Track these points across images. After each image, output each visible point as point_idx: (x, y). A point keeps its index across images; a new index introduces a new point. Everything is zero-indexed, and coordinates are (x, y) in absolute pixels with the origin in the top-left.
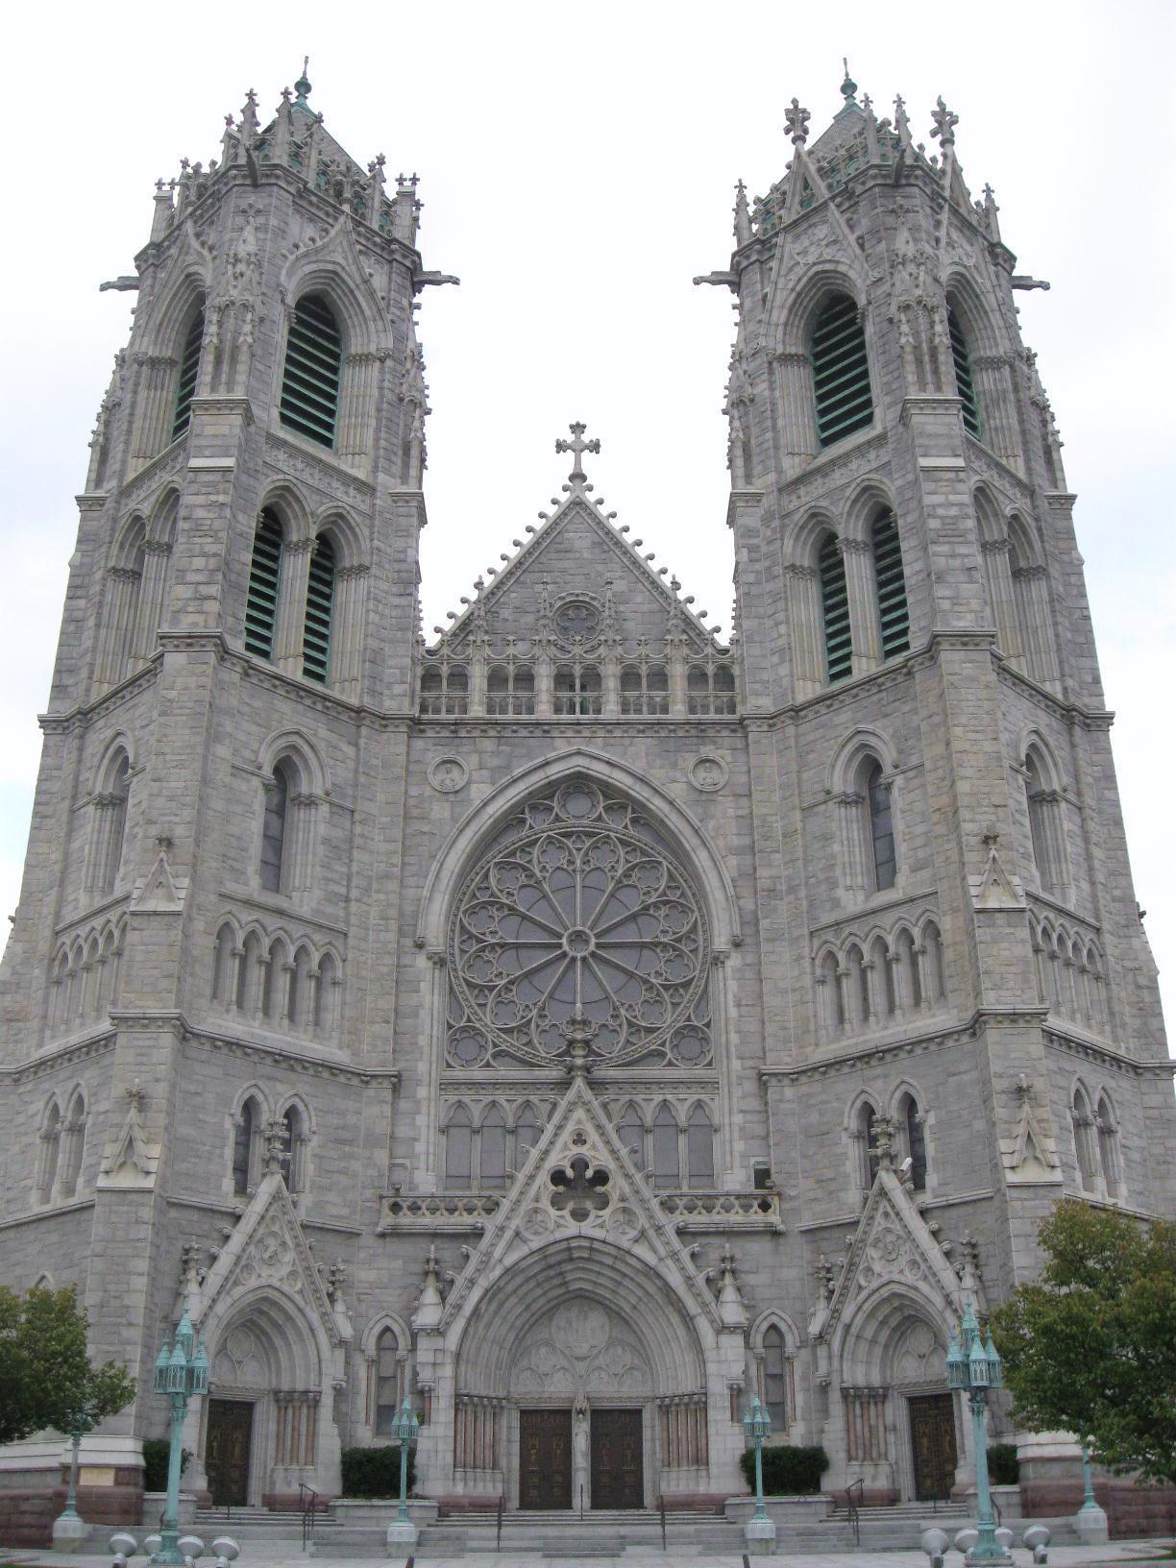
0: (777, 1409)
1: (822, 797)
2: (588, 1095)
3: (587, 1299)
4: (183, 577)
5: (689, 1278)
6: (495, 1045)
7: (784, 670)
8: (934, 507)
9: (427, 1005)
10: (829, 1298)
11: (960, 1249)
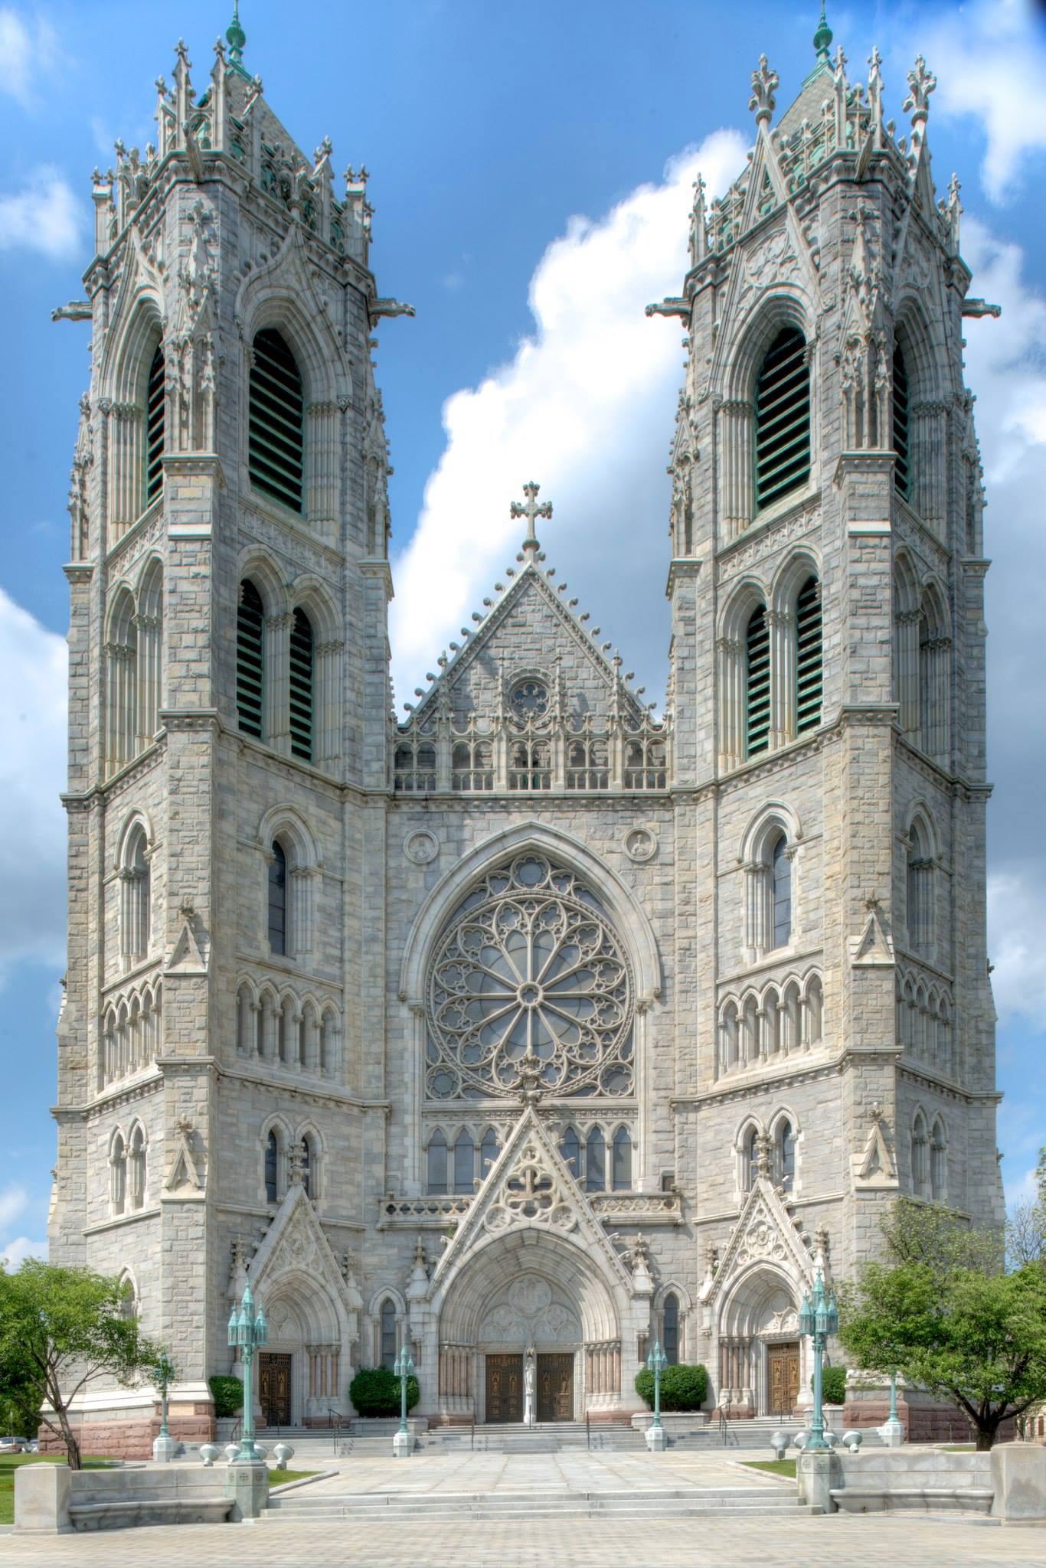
1: (734, 864)
3: (537, 1276)
9: (410, 1049)
10: (714, 1274)
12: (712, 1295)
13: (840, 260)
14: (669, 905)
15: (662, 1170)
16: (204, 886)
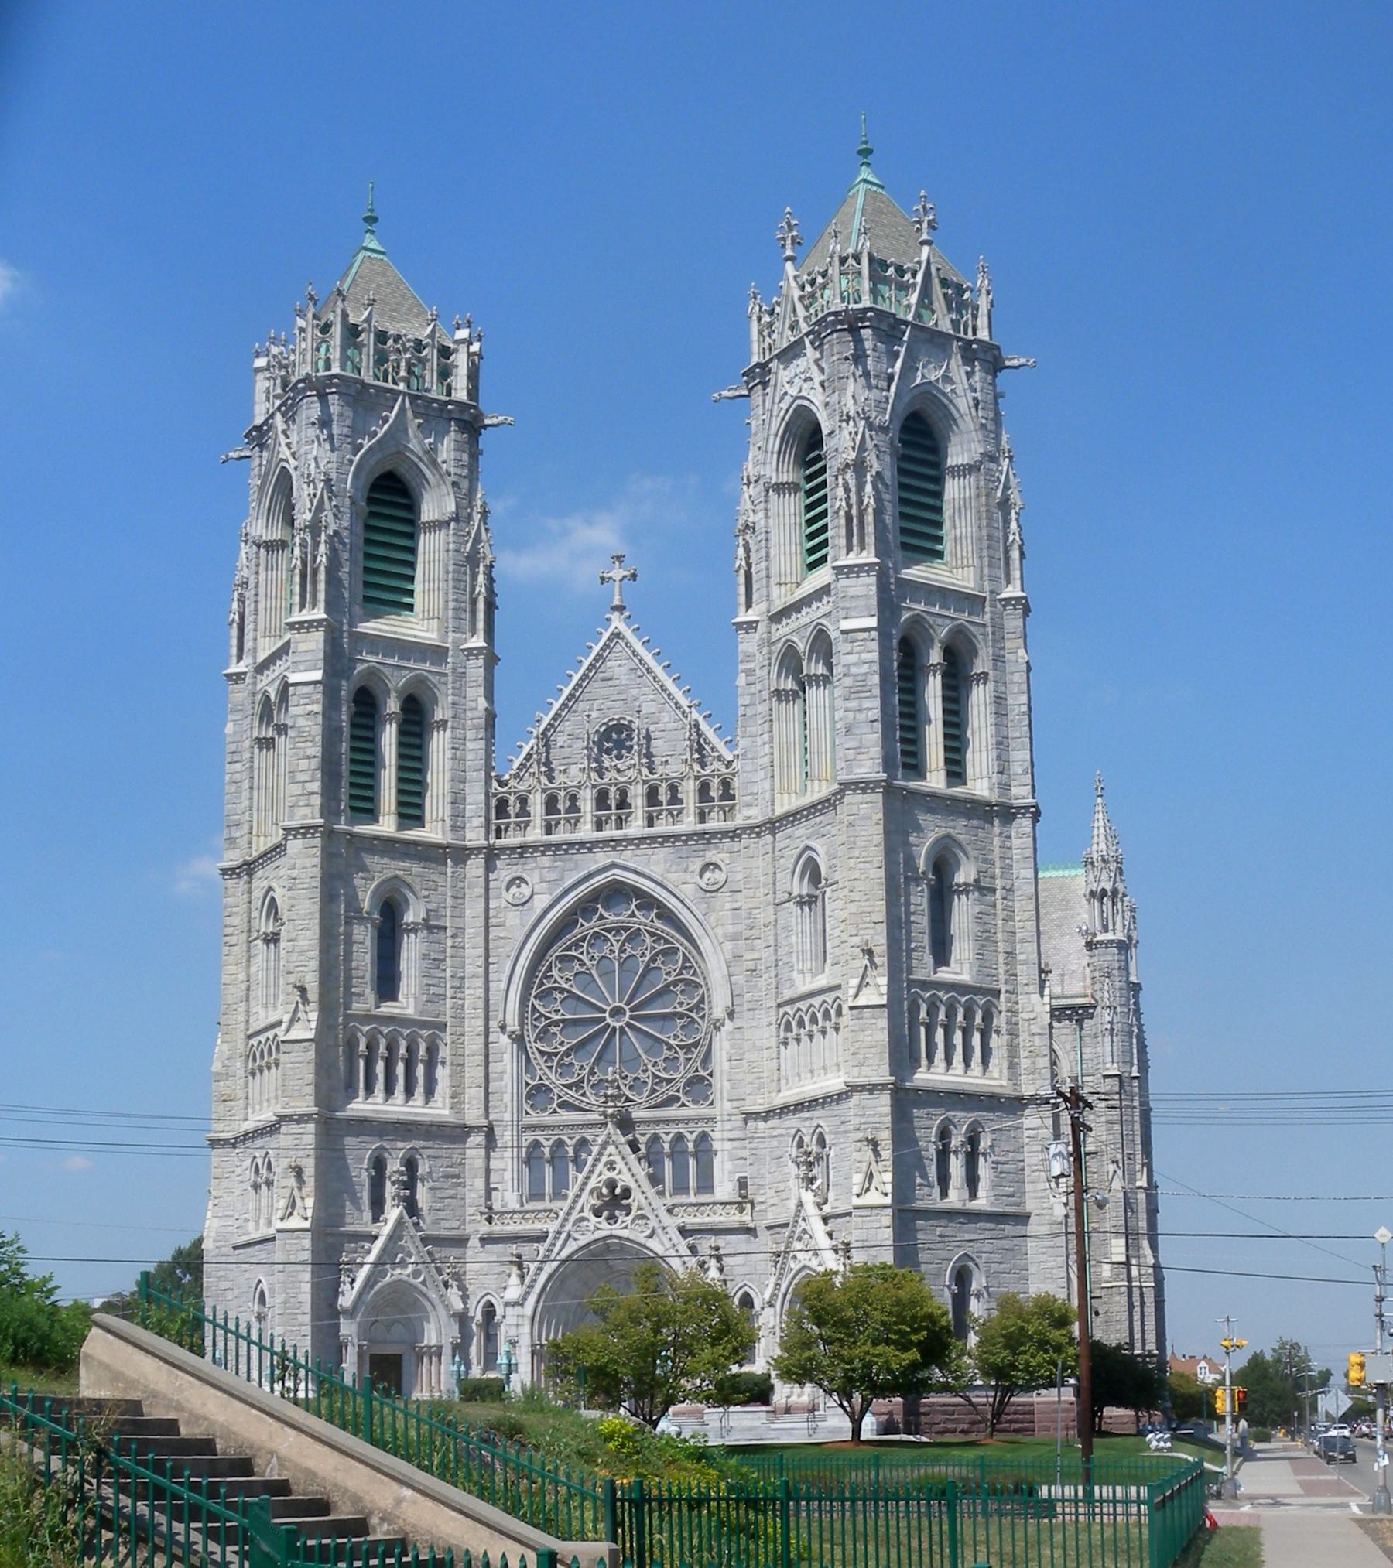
4: (293, 777)
6: (560, 1097)
8: (848, 666)
11: (840, 1246)
12: (774, 1295)
13: (837, 394)
15: (737, 1176)
16: (314, 964)
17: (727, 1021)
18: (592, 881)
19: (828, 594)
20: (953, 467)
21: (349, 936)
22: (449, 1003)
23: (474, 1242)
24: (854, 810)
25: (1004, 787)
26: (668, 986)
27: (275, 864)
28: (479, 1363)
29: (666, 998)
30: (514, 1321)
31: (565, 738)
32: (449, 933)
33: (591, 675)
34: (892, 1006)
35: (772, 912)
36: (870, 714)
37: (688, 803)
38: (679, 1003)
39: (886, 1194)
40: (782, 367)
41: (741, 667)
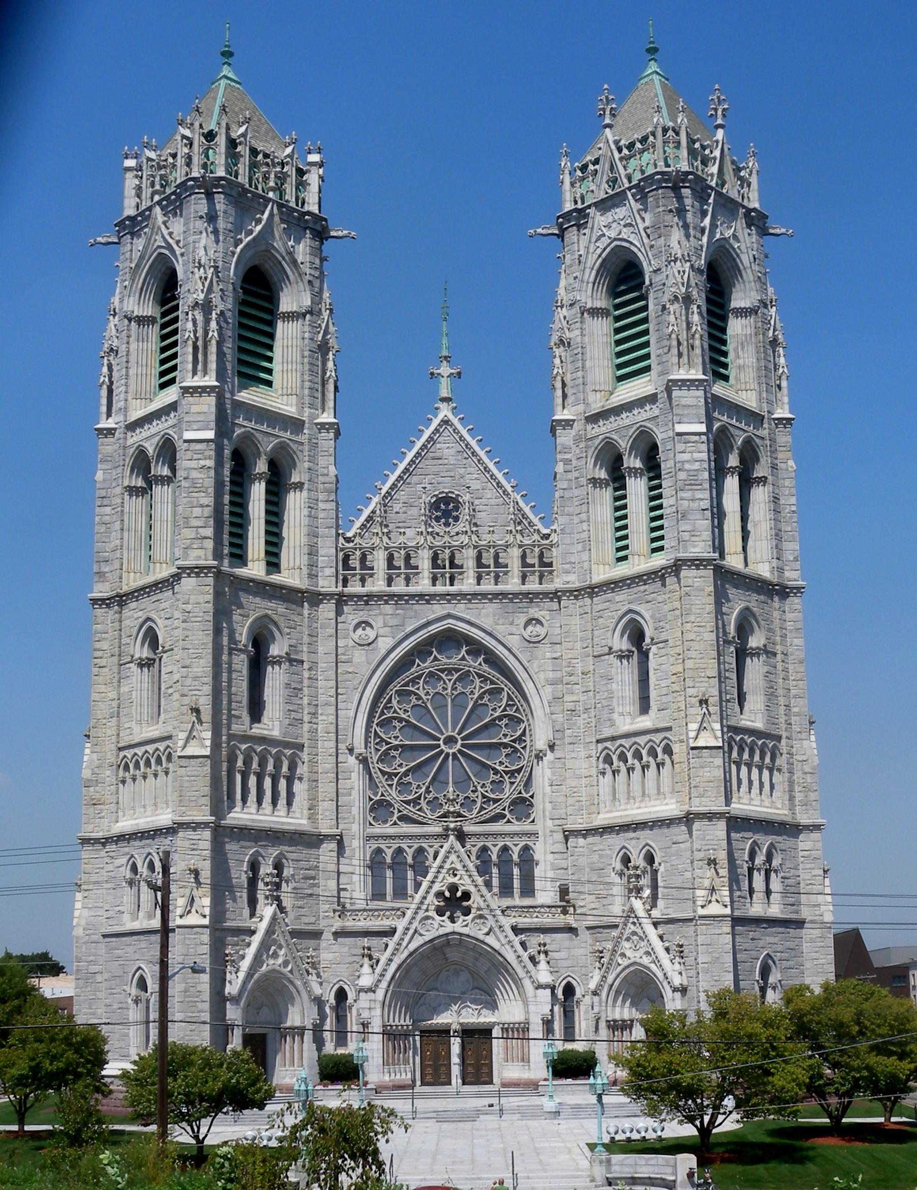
0: (569, 1035)
1: (606, 650)
2: (458, 845)
4: (187, 523)
5: (519, 957)
6: (400, 811)
7: (585, 556)
8: (683, 462)
11: (674, 947)
12: (600, 986)
13: (663, 238)
14: (558, 675)
16: (208, 689)
17: (549, 752)
18: (430, 628)
19: (175, 410)
20: (284, 313)
21: (230, 663)
22: (306, 727)
23: (327, 936)
24: (690, 582)
25: (312, 576)
26: (494, 720)
27: (155, 598)
28: (332, 1041)
29: (493, 730)
30: (367, 1005)
31: (401, 505)
32: (306, 666)
33: (423, 454)
34: (214, 758)
35: (592, 663)
36: (701, 503)
37: (512, 568)
38: (504, 735)
39: (205, 916)
40: (599, 214)
41: (559, 457)
